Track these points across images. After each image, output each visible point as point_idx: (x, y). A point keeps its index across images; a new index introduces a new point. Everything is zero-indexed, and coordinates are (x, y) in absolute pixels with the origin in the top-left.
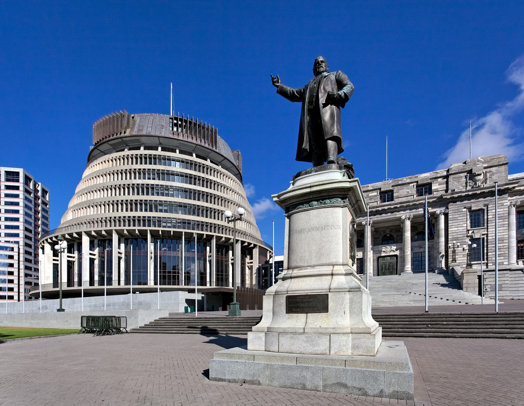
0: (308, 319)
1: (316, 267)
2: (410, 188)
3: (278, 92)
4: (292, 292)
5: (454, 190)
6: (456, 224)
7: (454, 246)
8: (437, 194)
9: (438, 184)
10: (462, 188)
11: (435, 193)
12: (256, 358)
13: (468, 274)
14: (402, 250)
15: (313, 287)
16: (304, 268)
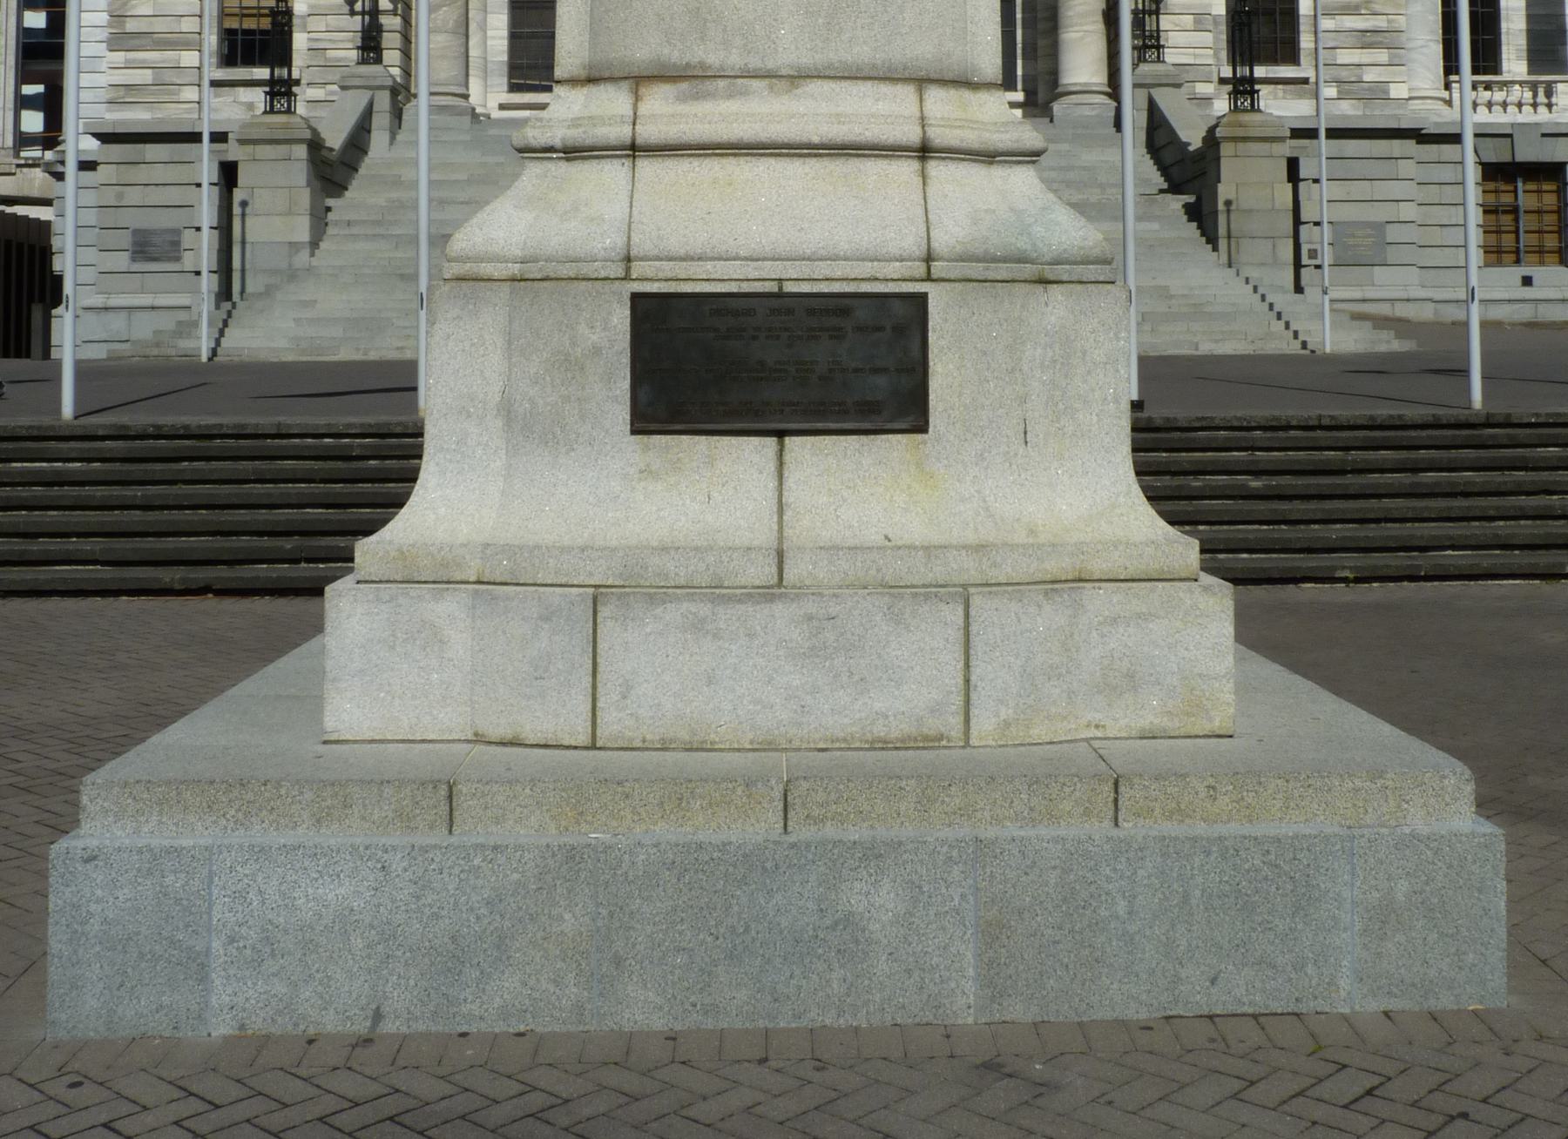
0: (790, 482)
1: (814, 87)
4: (668, 268)
13: (1241, 145)
14: (1542, 82)
16: (721, 83)
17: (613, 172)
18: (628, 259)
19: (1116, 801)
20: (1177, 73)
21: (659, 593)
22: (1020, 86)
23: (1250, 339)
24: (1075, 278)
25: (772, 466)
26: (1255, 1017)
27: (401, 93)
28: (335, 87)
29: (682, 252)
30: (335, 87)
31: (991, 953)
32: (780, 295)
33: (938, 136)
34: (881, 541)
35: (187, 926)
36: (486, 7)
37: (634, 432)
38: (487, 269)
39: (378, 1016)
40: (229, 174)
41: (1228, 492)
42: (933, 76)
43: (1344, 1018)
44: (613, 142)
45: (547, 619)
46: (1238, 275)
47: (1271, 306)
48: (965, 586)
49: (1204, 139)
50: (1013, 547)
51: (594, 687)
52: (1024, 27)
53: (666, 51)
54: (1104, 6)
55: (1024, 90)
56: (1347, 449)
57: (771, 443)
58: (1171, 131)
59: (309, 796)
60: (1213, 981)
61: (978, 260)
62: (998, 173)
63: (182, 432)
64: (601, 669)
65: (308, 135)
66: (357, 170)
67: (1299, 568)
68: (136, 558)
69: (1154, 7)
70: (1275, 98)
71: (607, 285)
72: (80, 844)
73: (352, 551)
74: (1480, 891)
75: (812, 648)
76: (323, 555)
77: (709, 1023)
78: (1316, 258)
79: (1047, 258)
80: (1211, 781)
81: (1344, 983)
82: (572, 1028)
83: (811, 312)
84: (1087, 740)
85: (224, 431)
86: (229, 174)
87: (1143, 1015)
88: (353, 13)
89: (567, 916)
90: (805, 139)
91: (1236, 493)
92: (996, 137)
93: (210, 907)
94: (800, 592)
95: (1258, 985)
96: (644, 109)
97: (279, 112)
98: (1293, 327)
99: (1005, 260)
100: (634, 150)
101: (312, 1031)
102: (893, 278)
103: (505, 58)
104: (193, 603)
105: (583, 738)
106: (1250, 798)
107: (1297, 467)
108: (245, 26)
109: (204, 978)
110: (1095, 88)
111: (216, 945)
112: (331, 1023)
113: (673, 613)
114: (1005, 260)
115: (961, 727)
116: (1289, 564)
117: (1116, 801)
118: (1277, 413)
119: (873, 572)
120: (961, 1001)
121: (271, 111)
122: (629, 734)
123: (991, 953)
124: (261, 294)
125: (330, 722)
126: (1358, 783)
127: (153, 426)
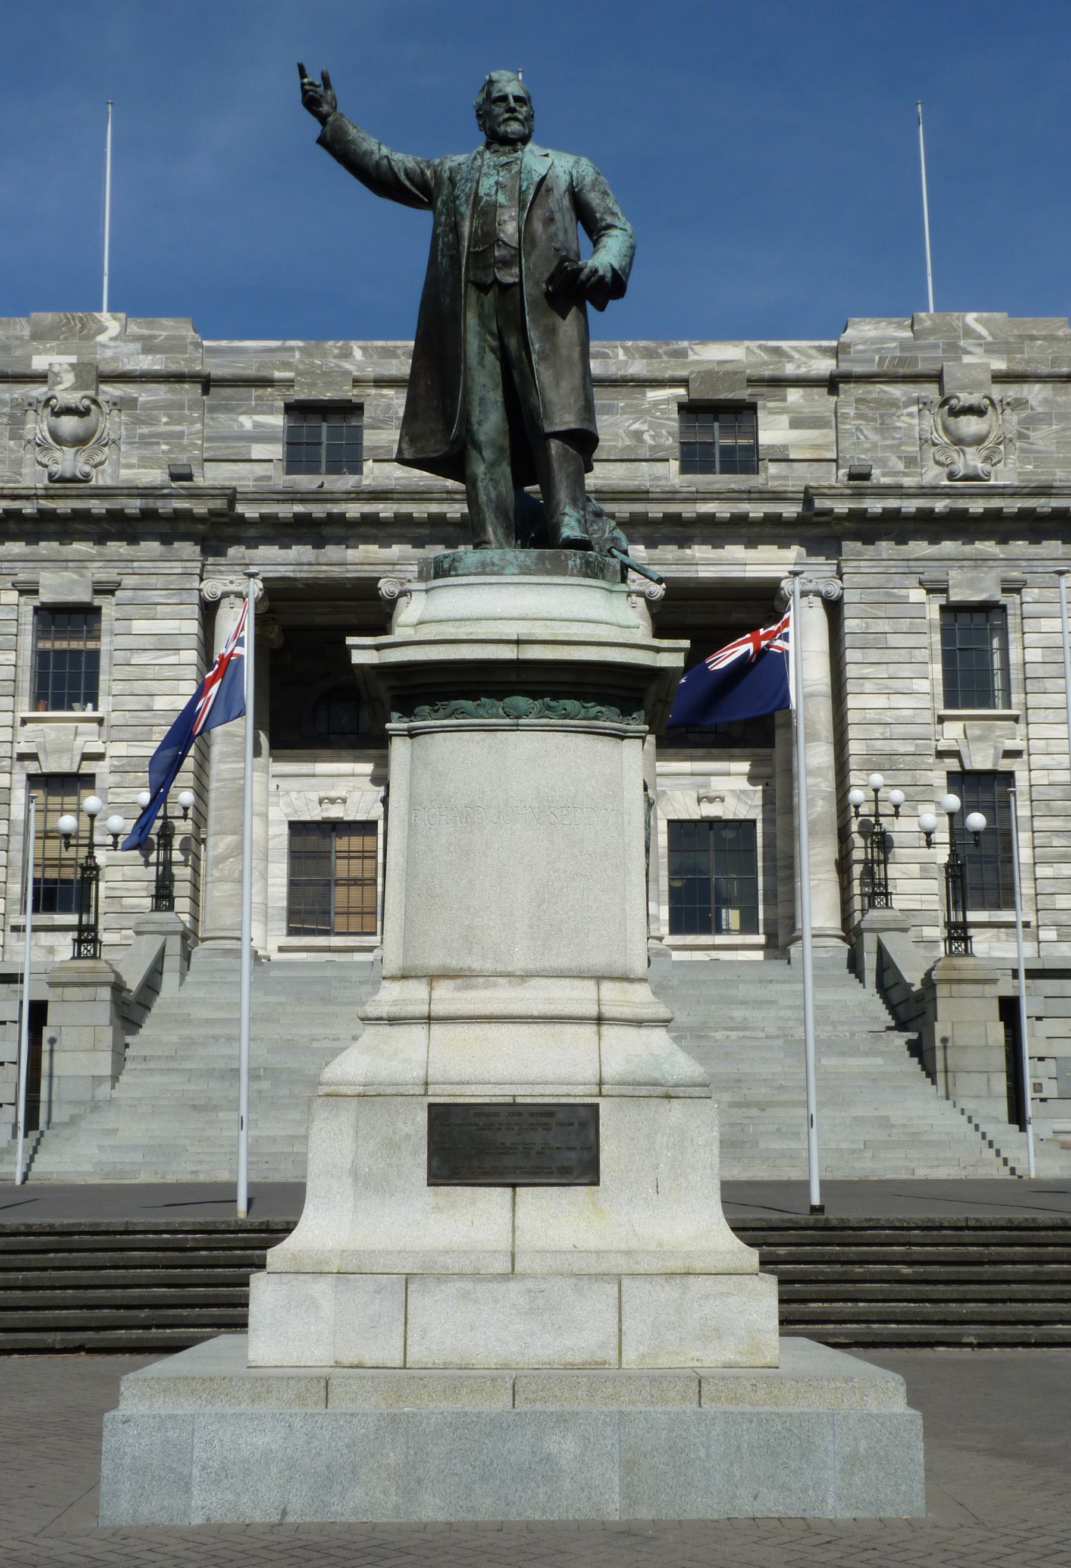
0: (519, 1214)
2: (647, 411)
3: (321, 141)
4: (449, 1089)
5: (866, 477)
6: (882, 671)
7: (876, 801)
8: (786, 478)
9: (785, 419)
10: (901, 466)
11: (773, 469)
12: (335, 1391)
13: (955, 987)
15: (533, 1073)
16: (481, 980)
17: (417, 1033)
18: (426, 1084)
19: (700, 1392)
20: (904, 918)
21: (444, 1277)
22: (761, 929)
23: (962, 1165)
24: (687, 1095)
25: (509, 1205)
26: (779, 1519)
27: (189, 938)
28: (131, 932)
29: (458, 1080)
30: (131, 932)
31: (629, 1479)
32: (514, 1104)
33: (608, 1011)
34: (571, 1248)
35: (179, 1460)
36: (267, 856)
37: (429, 1185)
38: (344, 1090)
39: (284, 1513)
40: (38, 1012)
41: (885, 1277)
42: (606, 975)
43: (831, 1521)
44: (418, 1015)
45: (379, 1292)
46: (955, 1106)
47: (984, 1136)
48: (619, 1275)
49: (923, 981)
50: (648, 1253)
51: (406, 1332)
52: (764, 875)
53: (448, 961)
54: (837, 856)
55: (765, 933)
56: (1040, 1262)
57: (509, 1190)
58: (898, 973)
59: (248, 1386)
60: (755, 1498)
61: (629, 1084)
62: (644, 1032)
63: (48, 1230)
64: (409, 1322)
65: (112, 978)
66: (150, 1009)
67: (934, 1335)
68: (23, 1325)
69: (882, 858)
70: (999, 940)
71: (415, 1099)
72: (121, 1413)
73: (264, 1257)
74: (908, 1448)
75: (531, 1309)
76: (169, 1322)
77: (470, 1518)
78: (1041, 1091)
79: (671, 1083)
80: (754, 1381)
81: (831, 1501)
82: (393, 1520)
83: (532, 1114)
84: (692, 1368)
85: (82, 1228)
86: (38, 1012)
87: (715, 1517)
88: (147, 864)
89: (391, 1455)
90: (529, 1014)
91: (890, 1278)
92: (643, 1011)
93: (192, 1450)
94: (524, 1276)
95: (781, 1501)
96: (436, 994)
97: (86, 958)
98: (1004, 1154)
99: (645, 1084)
100: (429, 1019)
101: (247, 1521)
102: (579, 1095)
103: (284, 904)
104: (71, 1358)
105: (399, 1363)
106: (776, 1392)
107: (943, 1259)
108: (47, 876)
109: (187, 1489)
110: (829, 932)
111: (195, 1471)
112: (258, 1517)
113: (452, 1288)
114: (645, 1084)
115: (616, 1356)
116: (928, 1331)
117: (700, 1392)
118: (931, 1216)
119: (566, 1266)
120: (612, 1507)
121: (78, 956)
122: (425, 1359)
123: (629, 1479)
124: (67, 1123)
125: (251, 1356)
126: (838, 1384)
127: (24, 1225)
